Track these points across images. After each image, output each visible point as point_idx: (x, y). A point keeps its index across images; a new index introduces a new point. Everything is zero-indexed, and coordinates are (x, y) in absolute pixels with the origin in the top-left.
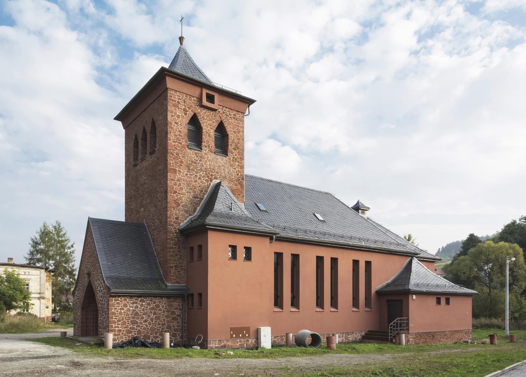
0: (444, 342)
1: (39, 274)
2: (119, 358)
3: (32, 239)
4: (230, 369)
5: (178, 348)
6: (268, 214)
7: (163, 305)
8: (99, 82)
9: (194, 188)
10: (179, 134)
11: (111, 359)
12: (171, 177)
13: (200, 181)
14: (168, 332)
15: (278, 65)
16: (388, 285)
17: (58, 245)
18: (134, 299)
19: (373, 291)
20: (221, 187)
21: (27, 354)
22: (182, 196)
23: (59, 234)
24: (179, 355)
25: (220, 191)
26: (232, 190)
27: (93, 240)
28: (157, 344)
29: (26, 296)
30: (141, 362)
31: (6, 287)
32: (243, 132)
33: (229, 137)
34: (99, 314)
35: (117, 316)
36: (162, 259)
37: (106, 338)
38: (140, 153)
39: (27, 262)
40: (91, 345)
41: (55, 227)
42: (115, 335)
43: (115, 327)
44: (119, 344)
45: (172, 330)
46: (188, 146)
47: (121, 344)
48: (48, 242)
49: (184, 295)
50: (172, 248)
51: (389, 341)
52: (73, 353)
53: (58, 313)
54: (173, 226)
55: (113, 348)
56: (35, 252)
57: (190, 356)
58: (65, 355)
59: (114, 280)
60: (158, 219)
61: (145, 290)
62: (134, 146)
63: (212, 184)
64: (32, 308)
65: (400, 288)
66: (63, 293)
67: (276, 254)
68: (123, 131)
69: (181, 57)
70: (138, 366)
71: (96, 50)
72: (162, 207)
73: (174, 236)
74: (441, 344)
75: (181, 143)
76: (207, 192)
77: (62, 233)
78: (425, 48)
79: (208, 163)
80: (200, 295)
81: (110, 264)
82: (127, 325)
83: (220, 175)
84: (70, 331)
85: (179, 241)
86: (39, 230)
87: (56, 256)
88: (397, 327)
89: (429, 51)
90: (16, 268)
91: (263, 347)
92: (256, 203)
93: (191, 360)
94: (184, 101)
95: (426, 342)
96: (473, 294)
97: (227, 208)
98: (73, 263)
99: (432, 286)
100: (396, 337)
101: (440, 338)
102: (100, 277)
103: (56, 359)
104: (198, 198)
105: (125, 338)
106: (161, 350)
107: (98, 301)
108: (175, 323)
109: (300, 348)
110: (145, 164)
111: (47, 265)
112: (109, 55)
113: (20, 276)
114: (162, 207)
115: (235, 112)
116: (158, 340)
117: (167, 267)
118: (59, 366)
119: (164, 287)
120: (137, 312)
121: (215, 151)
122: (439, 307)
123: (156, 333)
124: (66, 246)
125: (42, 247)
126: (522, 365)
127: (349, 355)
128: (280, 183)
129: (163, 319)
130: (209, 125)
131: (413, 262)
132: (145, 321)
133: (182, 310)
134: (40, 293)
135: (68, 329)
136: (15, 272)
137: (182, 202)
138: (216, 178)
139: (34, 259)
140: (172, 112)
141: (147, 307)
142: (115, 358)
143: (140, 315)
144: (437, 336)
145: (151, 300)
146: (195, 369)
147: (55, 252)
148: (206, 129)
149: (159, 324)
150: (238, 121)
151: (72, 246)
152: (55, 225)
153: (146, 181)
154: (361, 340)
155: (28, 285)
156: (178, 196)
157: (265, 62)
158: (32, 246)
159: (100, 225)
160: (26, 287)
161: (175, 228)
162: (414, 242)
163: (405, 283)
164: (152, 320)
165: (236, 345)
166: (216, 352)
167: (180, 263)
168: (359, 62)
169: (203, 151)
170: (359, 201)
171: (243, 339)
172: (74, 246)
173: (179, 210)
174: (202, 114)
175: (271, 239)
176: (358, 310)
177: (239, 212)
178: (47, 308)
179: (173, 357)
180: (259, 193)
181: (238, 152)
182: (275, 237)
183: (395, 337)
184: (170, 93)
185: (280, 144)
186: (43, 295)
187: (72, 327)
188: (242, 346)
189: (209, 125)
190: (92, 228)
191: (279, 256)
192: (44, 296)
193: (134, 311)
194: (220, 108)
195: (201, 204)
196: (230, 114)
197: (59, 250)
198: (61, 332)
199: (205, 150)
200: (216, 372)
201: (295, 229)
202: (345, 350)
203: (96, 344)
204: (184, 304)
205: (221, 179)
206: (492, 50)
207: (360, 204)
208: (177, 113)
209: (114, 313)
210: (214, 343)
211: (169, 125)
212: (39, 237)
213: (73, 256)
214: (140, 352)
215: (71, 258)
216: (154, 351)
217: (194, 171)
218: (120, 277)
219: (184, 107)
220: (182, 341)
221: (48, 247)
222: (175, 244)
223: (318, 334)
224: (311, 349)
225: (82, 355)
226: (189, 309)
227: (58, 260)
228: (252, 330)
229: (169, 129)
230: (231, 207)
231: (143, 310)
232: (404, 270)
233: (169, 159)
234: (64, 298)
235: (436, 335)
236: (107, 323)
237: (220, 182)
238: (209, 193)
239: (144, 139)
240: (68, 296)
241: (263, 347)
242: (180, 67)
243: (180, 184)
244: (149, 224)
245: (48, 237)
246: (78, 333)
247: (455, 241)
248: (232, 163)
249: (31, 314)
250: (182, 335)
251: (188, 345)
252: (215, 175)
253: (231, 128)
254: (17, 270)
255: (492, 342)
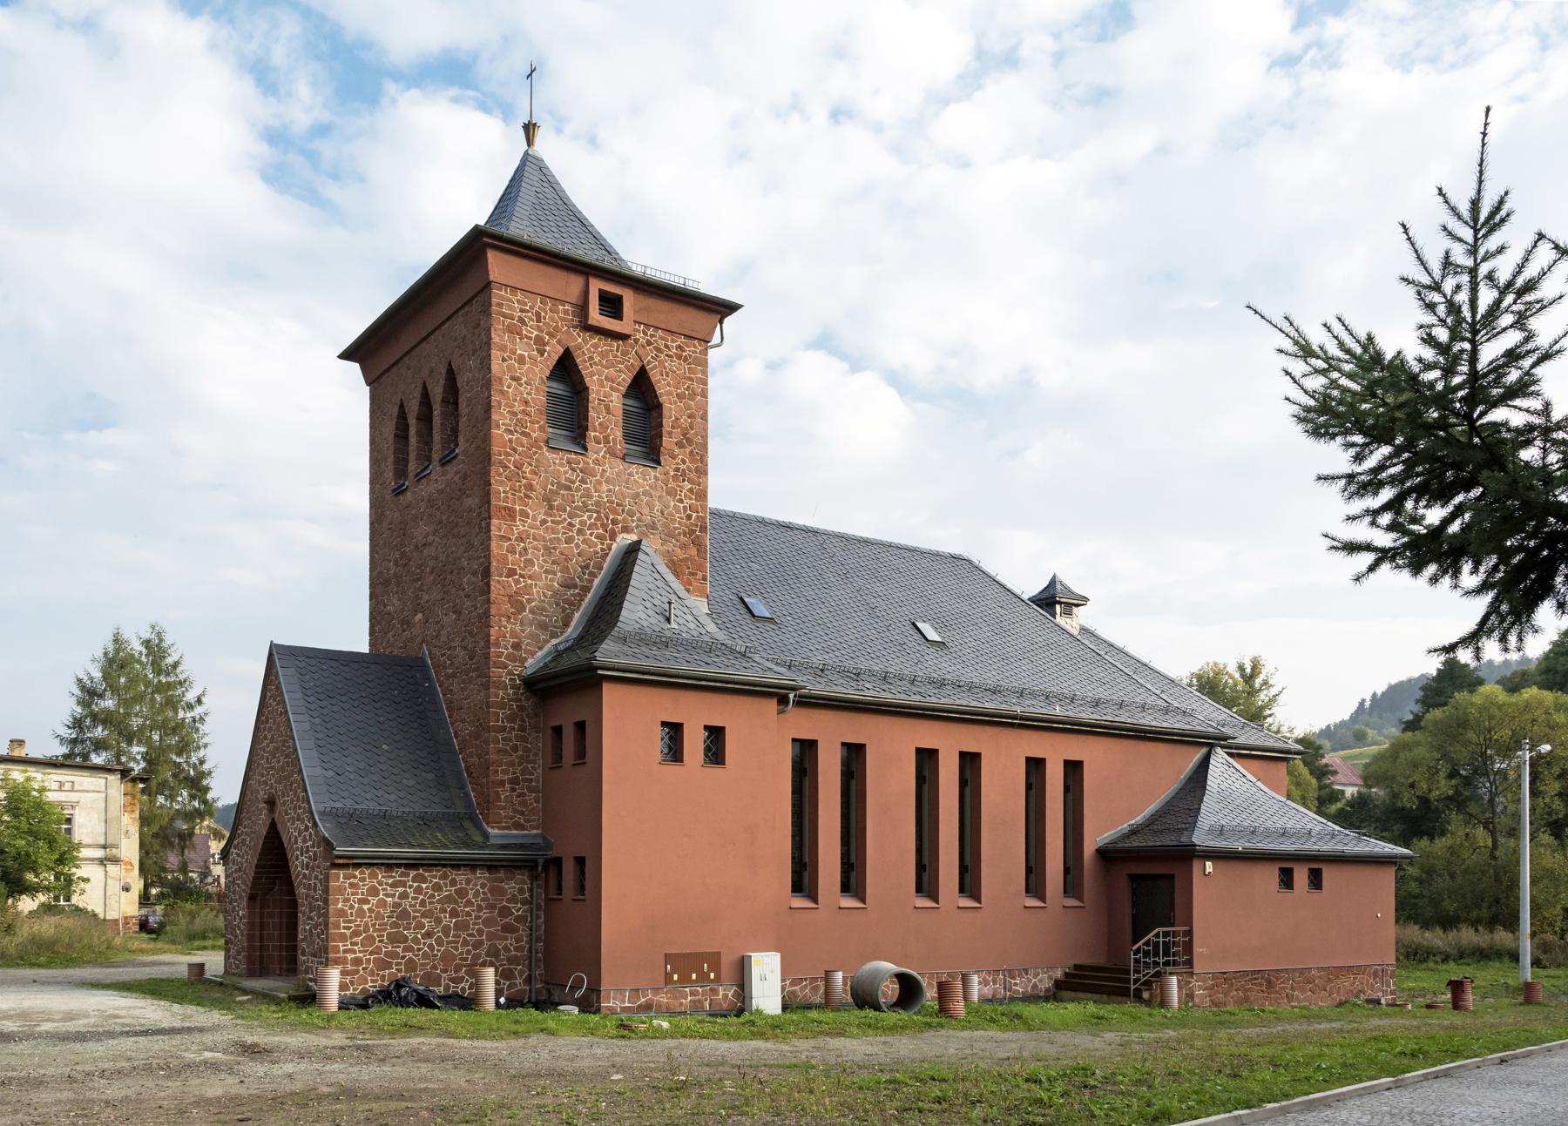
0: (1304, 1000)
1: (103, 789)
2: (360, 1037)
3: (80, 681)
4: (652, 1065)
5: (518, 1009)
6: (774, 627)
7: (477, 890)
8: (275, 176)
9: (566, 560)
10: (523, 410)
11: (338, 1039)
12: (500, 530)
13: (581, 538)
14: (491, 964)
15: (838, 114)
16: (1134, 832)
17: (158, 697)
18: (396, 875)
19: (1089, 848)
20: (641, 556)
21: (115, 1023)
22: (529, 582)
23: (159, 665)
24: (520, 1028)
25: (636, 568)
26: (673, 561)
27: (285, 707)
28: (458, 999)
29: (66, 857)
30: (421, 1046)
31: (8, 827)
32: (704, 395)
33: (665, 412)
34: (300, 915)
35: (351, 921)
36: (475, 760)
37: (319, 980)
38: (412, 456)
39: (64, 750)
40: (278, 1002)
41: (147, 643)
42: (343, 973)
43: (345, 951)
44: (354, 999)
45: (503, 960)
46: (547, 442)
47: (360, 997)
48: (127, 688)
49: (536, 862)
50: (503, 729)
51: (1129, 996)
52: (234, 1021)
53: (155, 904)
54: (506, 667)
55: (340, 1008)
56: (88, 720)
57: (551, 1033)
58: (215, 1028)
59: (343, 821)
60: (465, 648)
61: (427, 848)
62: (396, 436)
63: (614, 546)
64: (83, 892)
65: (1168, 840)
66: (172, 845)
67: (798, 744)
68: (365, 391)
69: (530, 182)
70: (413, 1054)
71: (264, 77)
72: (475, 614)
73: (508, 695)
74: (1293, 1007)
75: (527, 435)
76: (602, 568)
77: (170, 660)
78: (1319, 44)
79: (605, 487)
80: (580, 861)
81: (330, 773)
82: (377, 947)
83: (639, 520)
84: (214, 961)
85: (521, 708)
86: (99, 654)
87: (151, 732)
88: (1156, 954)
89: (1330, 59)
90: (34, 769)
91: (757, 1010)
92: (743, 595)
93: (551, 1042)
94: (538, 315)
95: (1246, 1000)
96: (1396, 856)
97: (656, 615)
98: (201, 753)
99: (1268, 833)
100: (1151, 985)
101: (1292, 988)
102: (305, 812)
103: (197, 1037)
104: (575, 586)
105: (373, 981)
106: (471, 1016)
107: (296, 878)
108: (510, 941)
109: (862, 1013)
110: (427, 489)
111: (123, 759)
112: (303, 90)
113: (48, 793)
114: (475, 614)
115: (681, 340)
116: (463, 989)
117: (488, 783)
118: (208, 1055)
119: (479, 839)
120: (405, 909)
121: (625, 451)
122: (1287, 895)
123: (458, 968)
124: (181, 701)
125: (109, 703)
126: (1479, 1067)
127: (999, 1034)
128: (815, 532)
129: (478, 930)
130: (607, 379)
131: (1211, 761)
132: (428, 935)
133: (531, 903)
134: (104, 847)
135: (195, 955)
136: (32, 783)
137: (529, 601)
138: (626, 530)
139: (83, 742)
140: (503, 348)
141: (434, 897)
142: (349, 1035)
143: (415, 917)
144: (1282, 983)
145: (444, 877)
146: (562, 1064)
147: (146, 718)
148: (599, 391)
149: (465, 943)
150: (689, 364)
151: (199, 701)
152: (146, 635)
153: (430, 538)
154: (1052, 992)
155: (69, 821)
156: (520, 583)
157: (796, 105)
158: (79, 703)
159: (304, 664)
160: (64, 826)
161: (510, 673)
162: (1271, 682)
163: (1183, 826)
164: (446, 931)
165: (682, 1004)
166: (622, 1021)
167: (523, 773)
168: (1101, 96)
169: (590, 453)
170: (1054, 576)
171: (701, 987)
172: (204, 699)
173: (522, 624)
174: (589, 349)
175: (783, 700)
176: (1043, 905)
177: (692, 626)
178: (126, 889)
179: (503, 1033)
180: (750, 564)
181: (691, 451)
182: (795, 696)
183: (1148, 983)
184: (498, 294)
185: (845, 366)
186: (114, 850)
187: (220, 948)
188: (699, 1005)
189: (607, 379)
190: (280, 673)
191: (806, 751)
192: (118, 856)
193: (396, 905)
194: (638, 331)
195: (584, 605)
196: (666, 346)
197: (159, 714)
198: (190, 965)
199: (596, 452)
200: (617, 1073)
201: (854, 671)
202: (992, 1021)
203: (292, 998)
204: (535, 886)
205: (642, 533)
206: (1544, 45)
207: (1059, 587)
208: (519, 352)
209: (342, 913)
210: (619, 996)
211: (495, 386)
212: (100, 675)
213: (201, 732)
214: (415, 1020)
215: (195, 736)
216: (454, 1017)
217: (565, 510)
218: (358, 812)
219: (536, 333)
220: (530, 990)
221: (123, 702)
222: (512, 719)
223: (914, 973)
224: (892, 1017)
225: (259, 1026)
226: (549, 900)
227: (158, 744)
228: (728, 960)
229: (495, 398)
230: (667, 614)
231: (423, 903)
232: (1185, 785)
233: (496, 481)
234: (173, 859)
235: (1278, 979)
236: (322, 940)
237: (639, 542)
238: (608, 571)
239: (426, 417)
240: (186, 852)
241: (757, 1010)
242: (527, 213)
243: (525, 549)
244: (439, 660)
245: (129, 674)
246: (237, 967)
247: (1416, 675)
248: (672, 484)
249: (81, 910)
250: (530, 976)
251: (545, 1003)
252: (624, 520)
253: (669, 385)
254: (38, 776)
255: (1457, 1004)
